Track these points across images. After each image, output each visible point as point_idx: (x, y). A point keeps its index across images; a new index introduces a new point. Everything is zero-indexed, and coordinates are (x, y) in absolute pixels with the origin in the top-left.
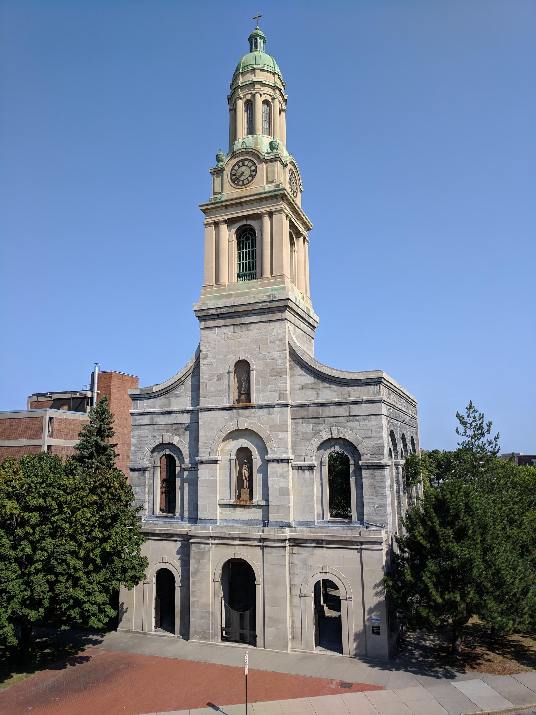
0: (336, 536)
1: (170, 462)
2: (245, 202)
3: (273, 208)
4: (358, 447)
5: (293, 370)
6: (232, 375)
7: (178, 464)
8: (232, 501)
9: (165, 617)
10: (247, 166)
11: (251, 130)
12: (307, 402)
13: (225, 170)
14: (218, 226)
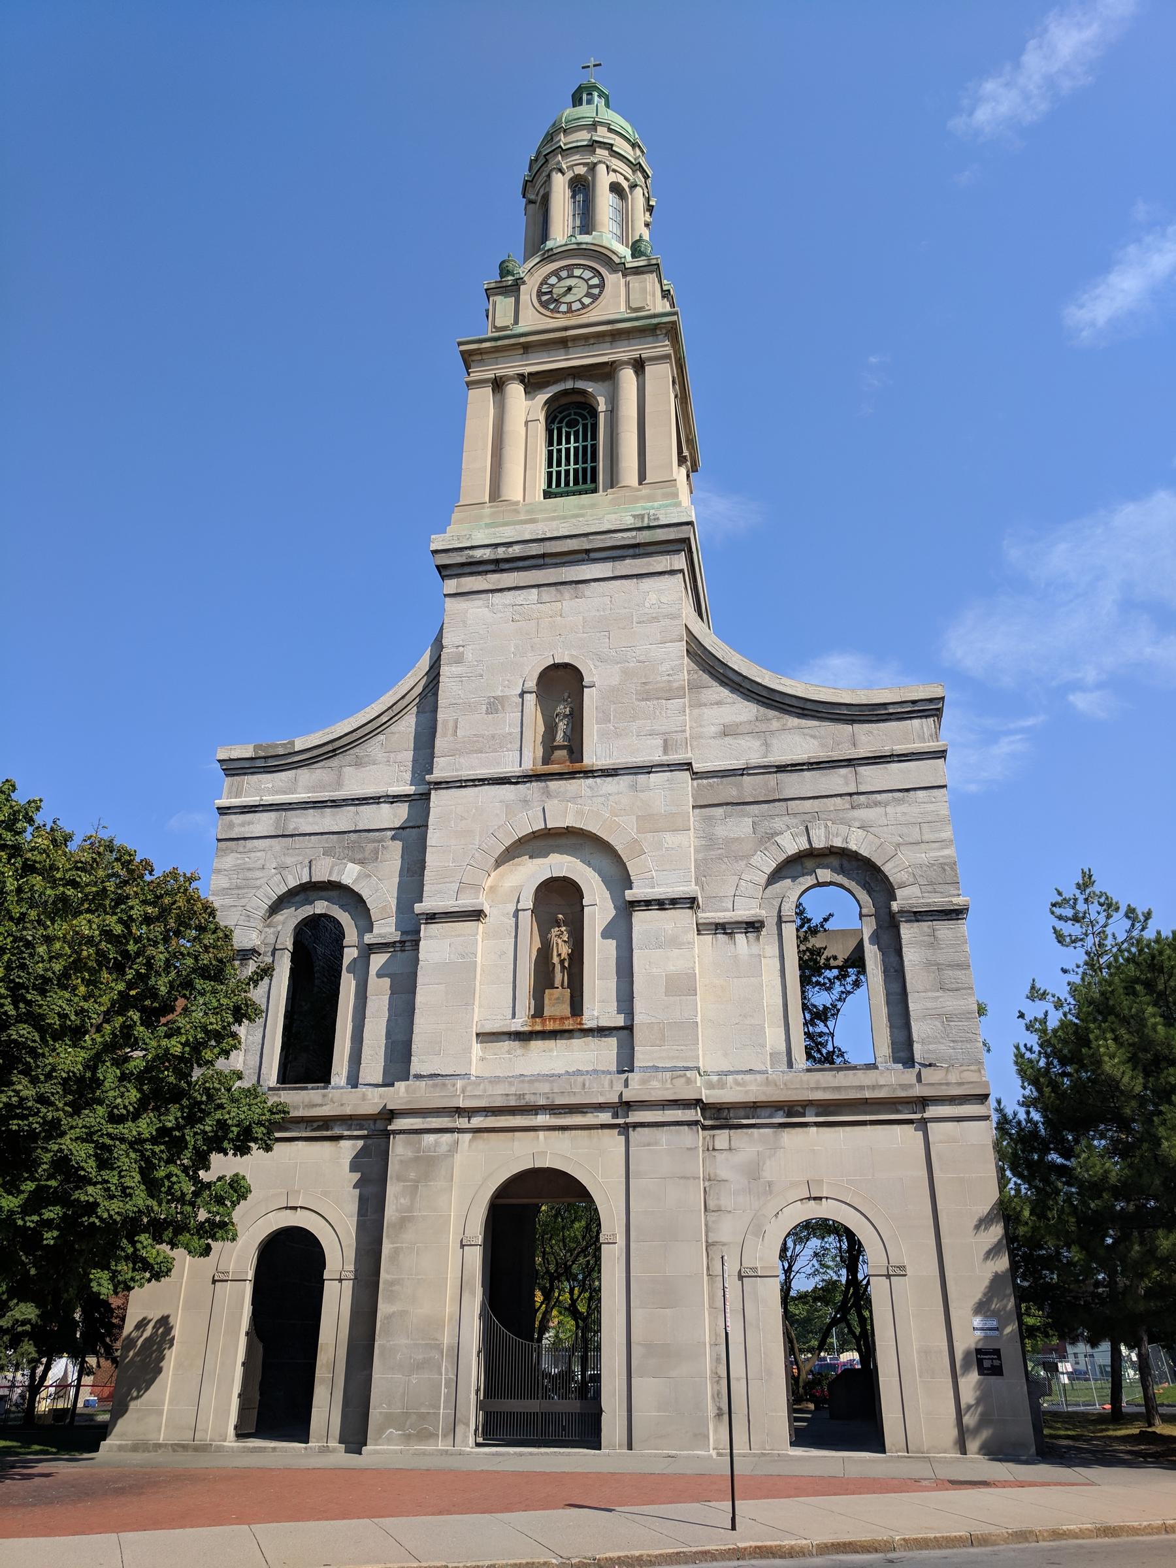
0: (846, 1088)
4: (886, 869)
6: (531, 699)
7: (351, 935)
9: (277, 1399)
10: (579, 277)
13: (524, 283)
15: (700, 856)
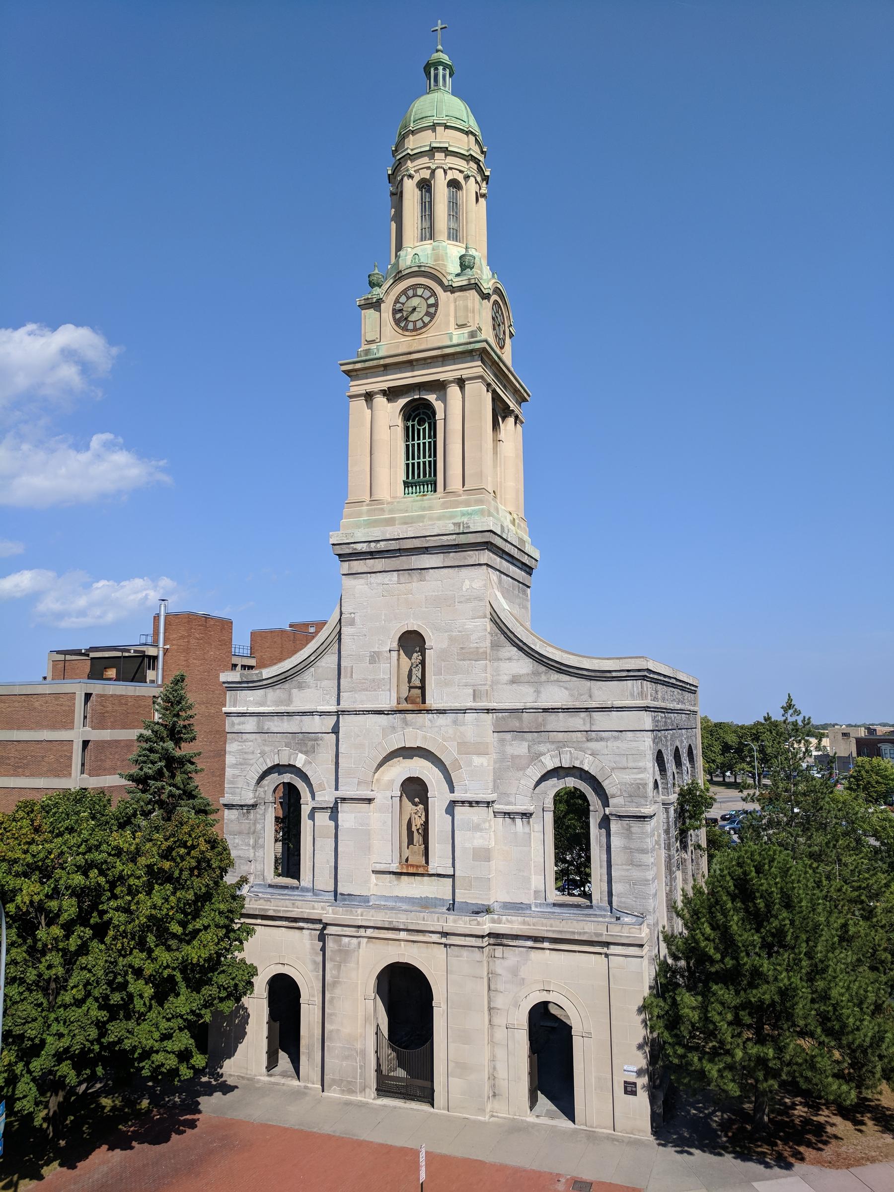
1: (290, 800)
2: (417, 360)
3: (465, 374)
4: (604, 784)
5: (498, 650)
8: (395, 867)
10: (421, 296)
11: (429, 233)
12: (520, 706)
14: (372, 400)
15: (497, 766)
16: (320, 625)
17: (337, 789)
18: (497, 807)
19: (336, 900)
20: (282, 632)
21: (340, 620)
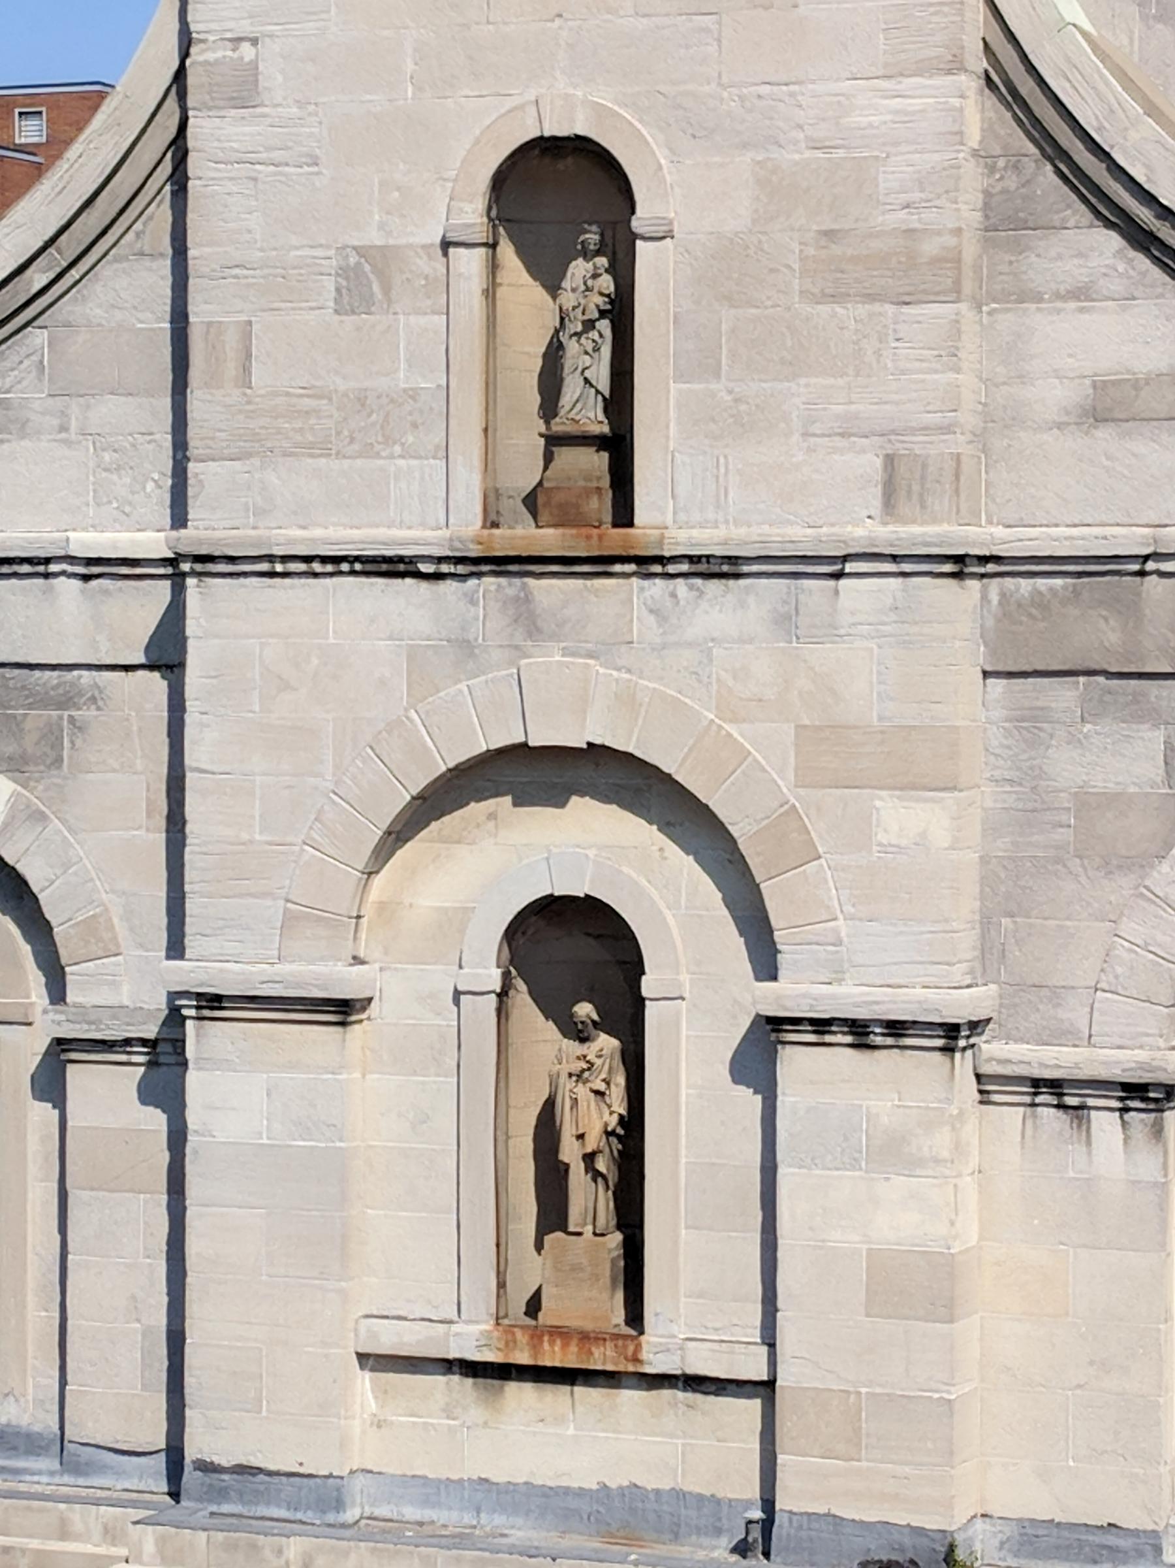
5: (1019, 248)
8: (472, 1339)
12: (1129, 540)
16: (75, 107)
17: (176, 948)
18: (994, 1051)
19: (175, 1495)
20: (578, 898)
21: (180, 75)
